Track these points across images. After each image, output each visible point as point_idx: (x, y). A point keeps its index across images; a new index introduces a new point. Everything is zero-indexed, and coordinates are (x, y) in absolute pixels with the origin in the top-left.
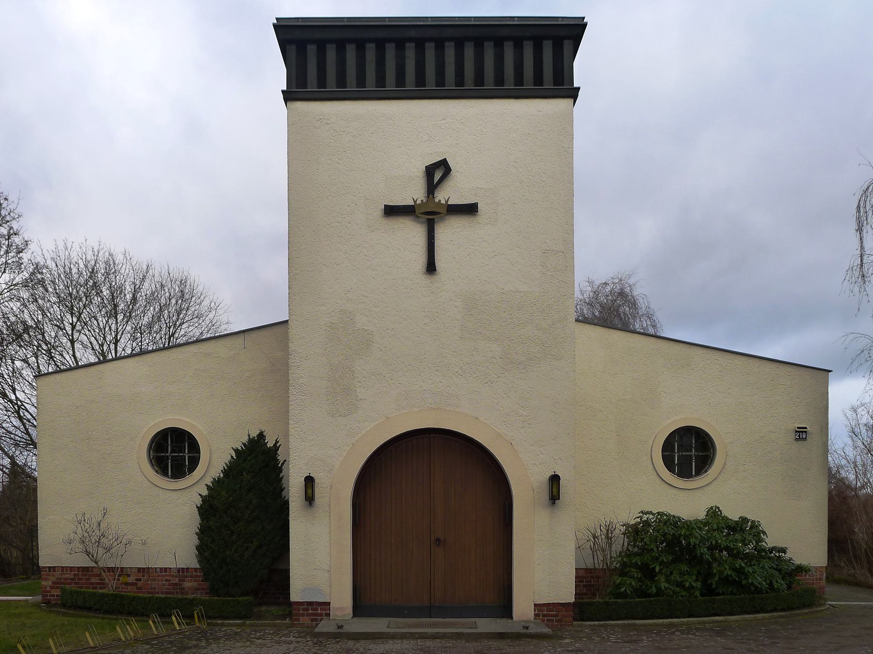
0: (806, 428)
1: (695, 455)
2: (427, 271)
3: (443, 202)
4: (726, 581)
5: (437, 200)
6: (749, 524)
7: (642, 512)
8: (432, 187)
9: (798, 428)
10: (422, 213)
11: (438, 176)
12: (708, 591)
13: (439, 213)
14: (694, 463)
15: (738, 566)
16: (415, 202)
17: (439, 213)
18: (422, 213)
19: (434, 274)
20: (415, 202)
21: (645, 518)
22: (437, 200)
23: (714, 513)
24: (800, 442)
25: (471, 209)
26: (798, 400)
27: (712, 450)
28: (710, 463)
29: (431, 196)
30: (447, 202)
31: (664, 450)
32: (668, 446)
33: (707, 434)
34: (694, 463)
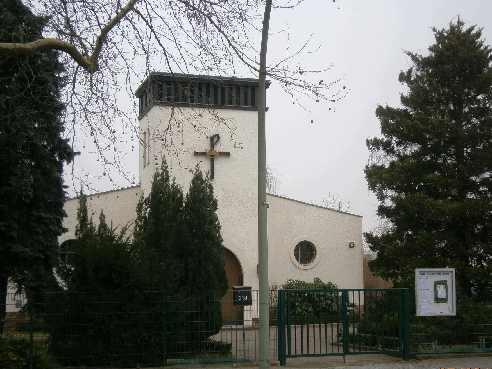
0: (353, 242)
1: (308, 254)
2: (279, 292)
3: (217, 151)
4: (324, 309)
5: (215, 151)
6: (332, 285)
7: (288, 280)
8: (212, 145)
9: (350, 242)
10: (209, 156)
11: (215, 140)
12: (317, 313)
13: (215, 156)
14: (307, 258)
15: (328, 303)
16: (206, 151)
17: (215, 156)
18: (209, 156)
19: (66, 45)
20: (206, 151)
21: (289, 282)
22: (215, 151)
23: (317, 280)
24: (351, 249)
25: (228, 154)
26: (350, 230)
27: (315, 252)
28: (315, 258)
29: (212, 149)
30: (219, 151)
31: (295, 251)
32: (296, 250)
33: (313, 245)
34: (307, 258)
